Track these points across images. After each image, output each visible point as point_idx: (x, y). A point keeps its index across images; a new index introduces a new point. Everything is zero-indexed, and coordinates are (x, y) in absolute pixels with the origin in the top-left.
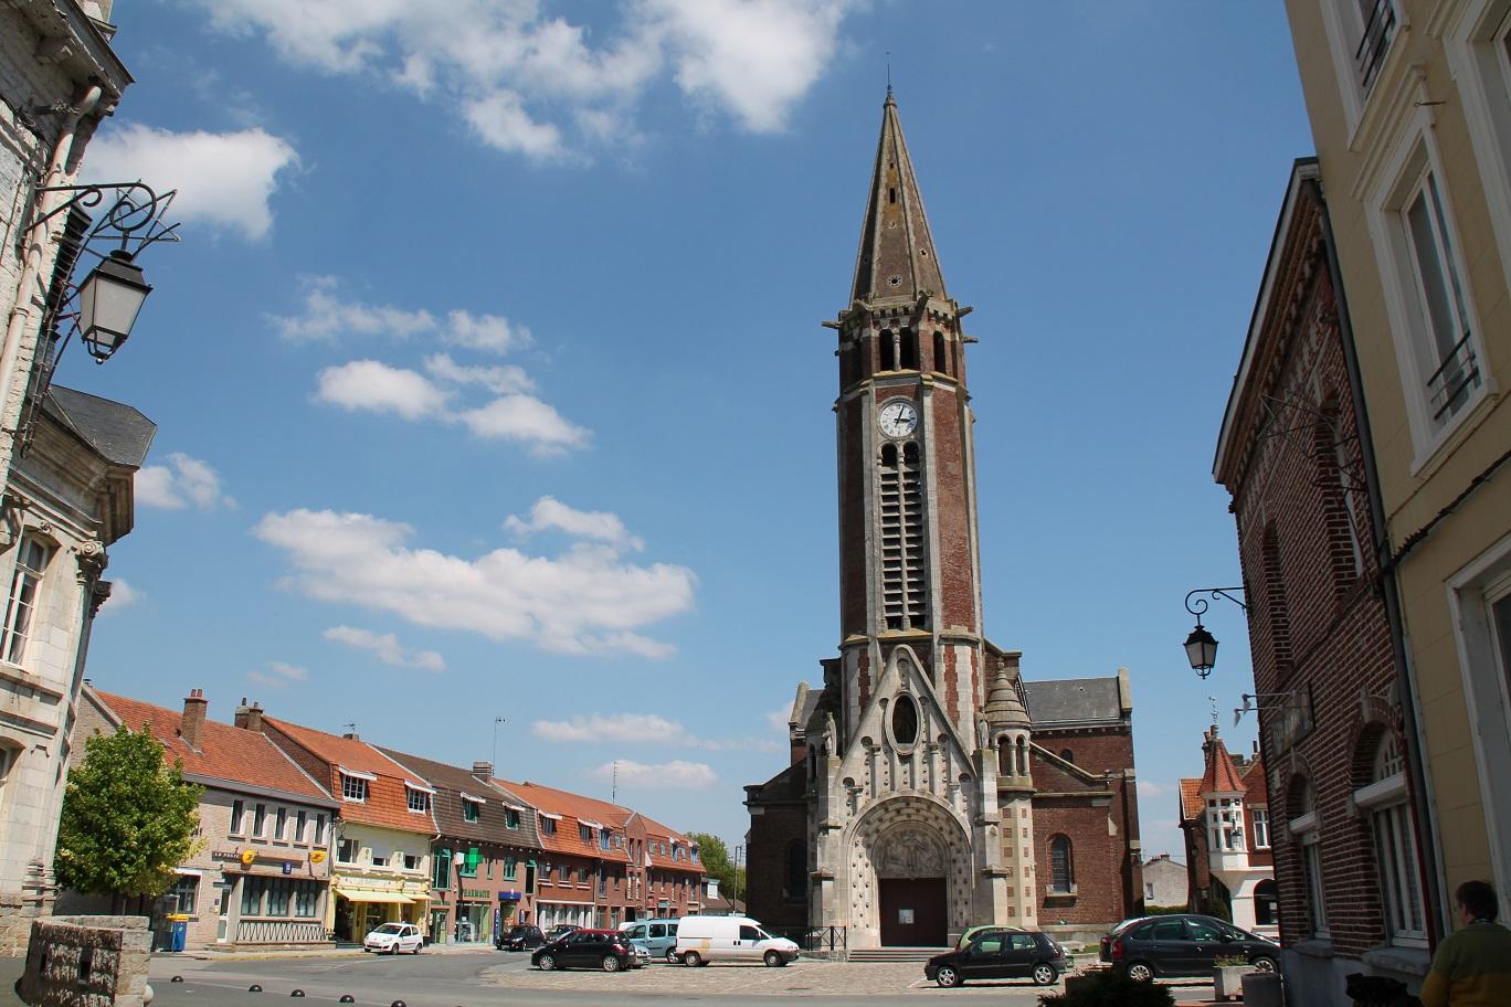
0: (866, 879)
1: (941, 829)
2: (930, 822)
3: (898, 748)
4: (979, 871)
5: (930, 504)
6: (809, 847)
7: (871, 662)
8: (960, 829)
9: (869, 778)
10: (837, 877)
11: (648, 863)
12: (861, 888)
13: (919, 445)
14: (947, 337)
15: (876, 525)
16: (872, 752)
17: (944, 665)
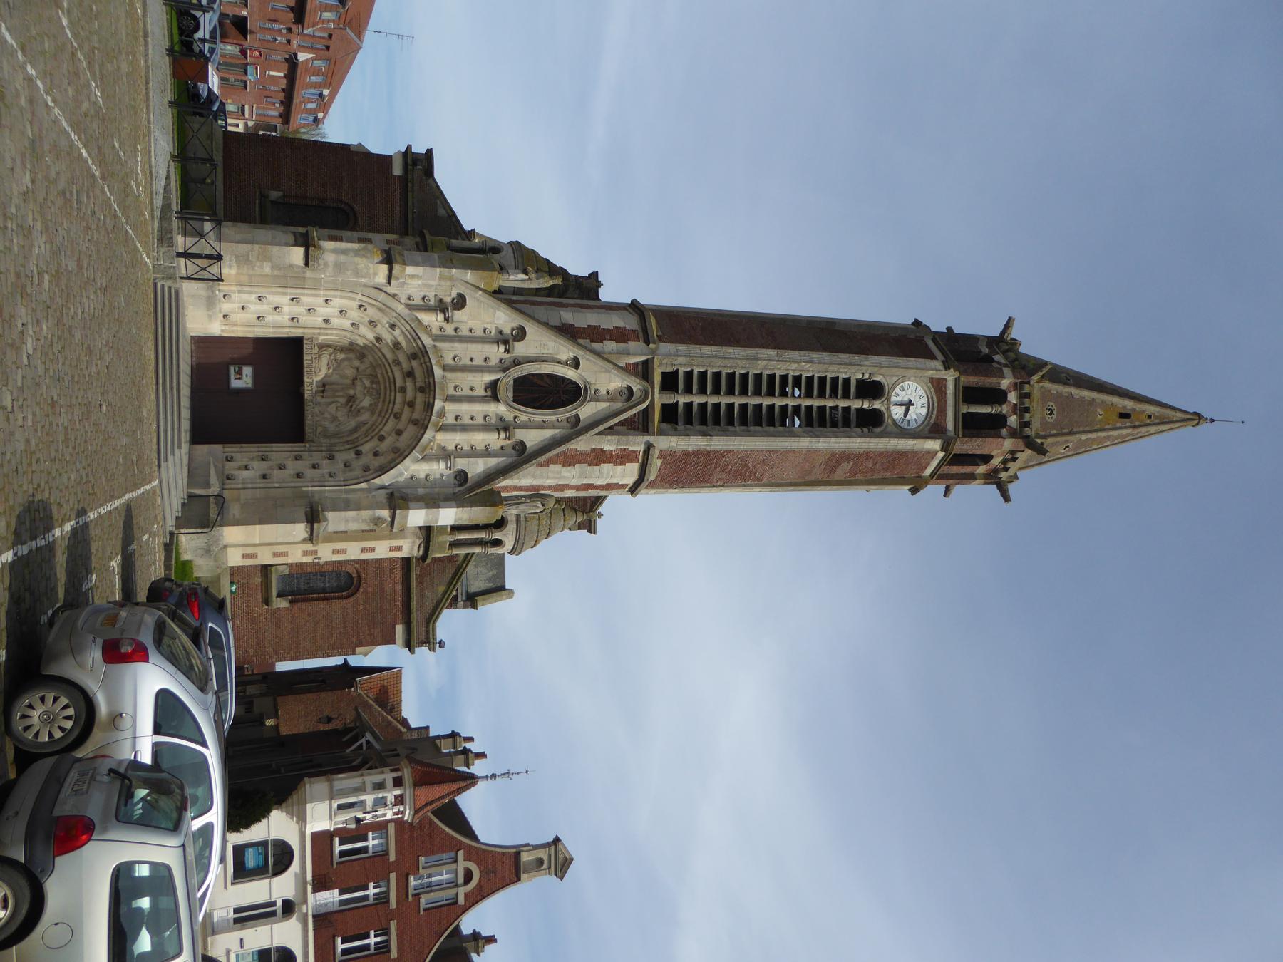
0: (303, 319)
1: (382, 438)
2: (391, 423)
3: (507, 380)
4: (316, 498)
5: (814, 440)
6: (349, 233)
7: (622, 345)
8: (383, 470)
9: (465, 332)
10: (309, 274)
11: (302, 56)
12: (288, 309)
13: (877, 430)
14: (981, 469)
15: (794, 366)
16: (503, 340)
17: (612, 448)
